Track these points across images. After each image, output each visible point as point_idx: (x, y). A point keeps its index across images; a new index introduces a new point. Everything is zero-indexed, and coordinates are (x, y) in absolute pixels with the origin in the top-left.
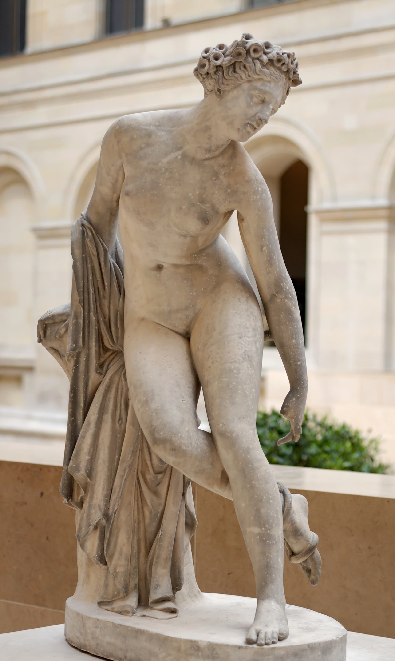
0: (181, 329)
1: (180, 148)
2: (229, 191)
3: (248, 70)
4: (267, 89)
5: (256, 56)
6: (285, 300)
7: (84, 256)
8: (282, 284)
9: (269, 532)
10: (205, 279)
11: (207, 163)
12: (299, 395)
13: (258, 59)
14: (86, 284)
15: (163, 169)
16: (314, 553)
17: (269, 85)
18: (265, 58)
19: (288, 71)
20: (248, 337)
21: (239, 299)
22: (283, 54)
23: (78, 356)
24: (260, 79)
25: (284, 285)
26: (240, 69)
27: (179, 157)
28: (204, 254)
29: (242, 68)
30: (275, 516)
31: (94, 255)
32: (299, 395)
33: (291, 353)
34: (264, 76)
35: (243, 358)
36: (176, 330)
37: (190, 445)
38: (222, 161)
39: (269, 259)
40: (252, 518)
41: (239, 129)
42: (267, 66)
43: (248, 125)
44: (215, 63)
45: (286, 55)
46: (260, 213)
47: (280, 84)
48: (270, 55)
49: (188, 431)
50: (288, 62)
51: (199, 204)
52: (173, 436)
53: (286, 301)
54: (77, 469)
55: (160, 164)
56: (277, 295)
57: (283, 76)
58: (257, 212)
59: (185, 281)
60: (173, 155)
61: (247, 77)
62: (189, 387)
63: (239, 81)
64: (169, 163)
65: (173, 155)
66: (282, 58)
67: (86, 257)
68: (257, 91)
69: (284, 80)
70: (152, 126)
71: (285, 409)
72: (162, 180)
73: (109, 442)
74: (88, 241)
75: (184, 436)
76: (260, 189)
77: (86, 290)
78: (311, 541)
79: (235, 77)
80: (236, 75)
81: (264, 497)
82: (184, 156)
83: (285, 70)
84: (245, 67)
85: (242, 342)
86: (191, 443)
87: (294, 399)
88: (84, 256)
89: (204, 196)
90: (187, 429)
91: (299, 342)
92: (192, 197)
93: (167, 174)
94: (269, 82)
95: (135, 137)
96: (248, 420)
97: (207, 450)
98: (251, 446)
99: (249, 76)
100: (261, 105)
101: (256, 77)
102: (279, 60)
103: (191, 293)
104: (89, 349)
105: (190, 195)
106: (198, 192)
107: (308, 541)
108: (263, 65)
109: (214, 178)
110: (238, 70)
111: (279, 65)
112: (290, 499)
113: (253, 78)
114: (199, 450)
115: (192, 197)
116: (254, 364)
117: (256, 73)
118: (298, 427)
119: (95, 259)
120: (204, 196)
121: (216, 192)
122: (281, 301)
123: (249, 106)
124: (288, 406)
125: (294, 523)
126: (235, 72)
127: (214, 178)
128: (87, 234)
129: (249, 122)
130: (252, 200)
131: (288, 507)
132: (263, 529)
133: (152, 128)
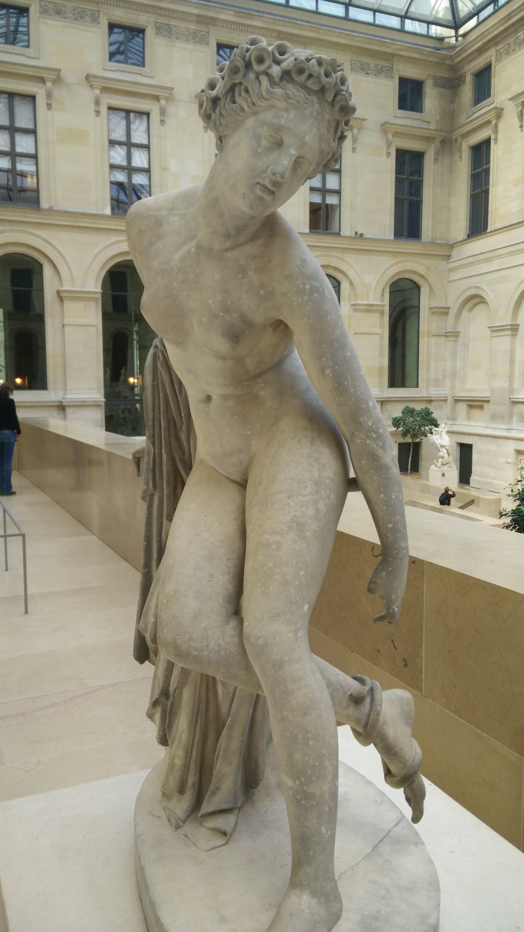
0: (237, 477)
1: (194, 237)
2: (262, 292)
3: (250, 96)
4: (283, 122)
5: (262, 68)
6: (366, 441)
7: (155, 383)
8: (362, 419)
9: (305, 788)
10: (261, 413)
11: (229, 254)
12: (390, 569)
13: (266, 74)
14: (157, 416)
15: (176, 268)
16: (413, 781)
17: (286, 115)
18: (276, 70)
19: (323, 90)
20: (304, 496)
21: (299, 441)
22: (308, 60)
23: (152, 496)
24: (272, 107)
25: (364, 420)
26: (240, 95)
27: (193, 250)
28: (261, 381)
29: (243, 93)
30: (317, 764)
31: (166, 382)
32: (390, 569)
33: (379, 512)
34: (277, 101)
35: (290, 528)
36: (232, 478)
37: (205, 649)
38: (251, 249)
39: (336, 385)
40: (284, 763)
41: (244, 194)
42: (281, 84)
43: (258, 186)
44: (210, 94)
45: (314, 61)
46: (311, 322)
47: (307, 112)
48: (284, 65)
49: (205, 629)
50: (320, 74)
51: (221, 314)
52: (178, 637)
53: (368, 441)
54: (146, 628)
55: (172, 262)
56: (356, 433)
57: (314, 98)
58: (306, 320)
59: (236, 417)
60: (185, 248)
61: (251, 107)
62: (228, 559)
63: (239, 115)
64: (182, 259)
65: (185, 248)
66: (306, 67)
67: (158, 384)
68: (266, 128)
69: (317, 105)
70: (163, 211)
71: (372, 586)
72: (175, 284)
73: (227, 577)
74: (159, 364)
75: (195, 637)
76: (307, 287)
77: (156, 423)
78: (409, 764)
79: (233, 110)
80: (234, 106)
81: (300, 737)
82: (199, 248)
83: (316, 88)
84: (247, 91)
85: (292, 504)
86: (207, 646)
87: (384, 574)
88: (155, 383)
89: (229, 302)
90: (203, 625)
91: (391, 497)
92: (213, 306)
93: (180, 275)
94: (287, 110)
95: (143, 228)
96: (288, 617)
97: (236, 652)
98: (286, 658)
99: (254, 104)
100: (277, 152)
101: (263, 104)
102: (301, 71)
103: (244, 432)
104: (162, 491)
105: (210, 302)
106: (219, 298)
107: (405, 765)
108: (273, 83)
109: (240, 276)
110: (237, 98)
111: (302, 78)
112: (379, 708)
113: (260, 107)
114: (222, 653)
115: (213, 306)
116: (308, 534)
117: (263, 98)
118: (391, 611)
119: (167, 386)
120: (229, 302)
121: (245, 296)
122: (361, 442)
123: (255, 154)
124: (375, 583)
125: (385, 738)
126: (234, 102)
127: (240, 276)
128: (159, 357)
129: (258, 181)
130: (296, 303)
131: (373, 719)
132: (297, 782)
133: (163, 212)
